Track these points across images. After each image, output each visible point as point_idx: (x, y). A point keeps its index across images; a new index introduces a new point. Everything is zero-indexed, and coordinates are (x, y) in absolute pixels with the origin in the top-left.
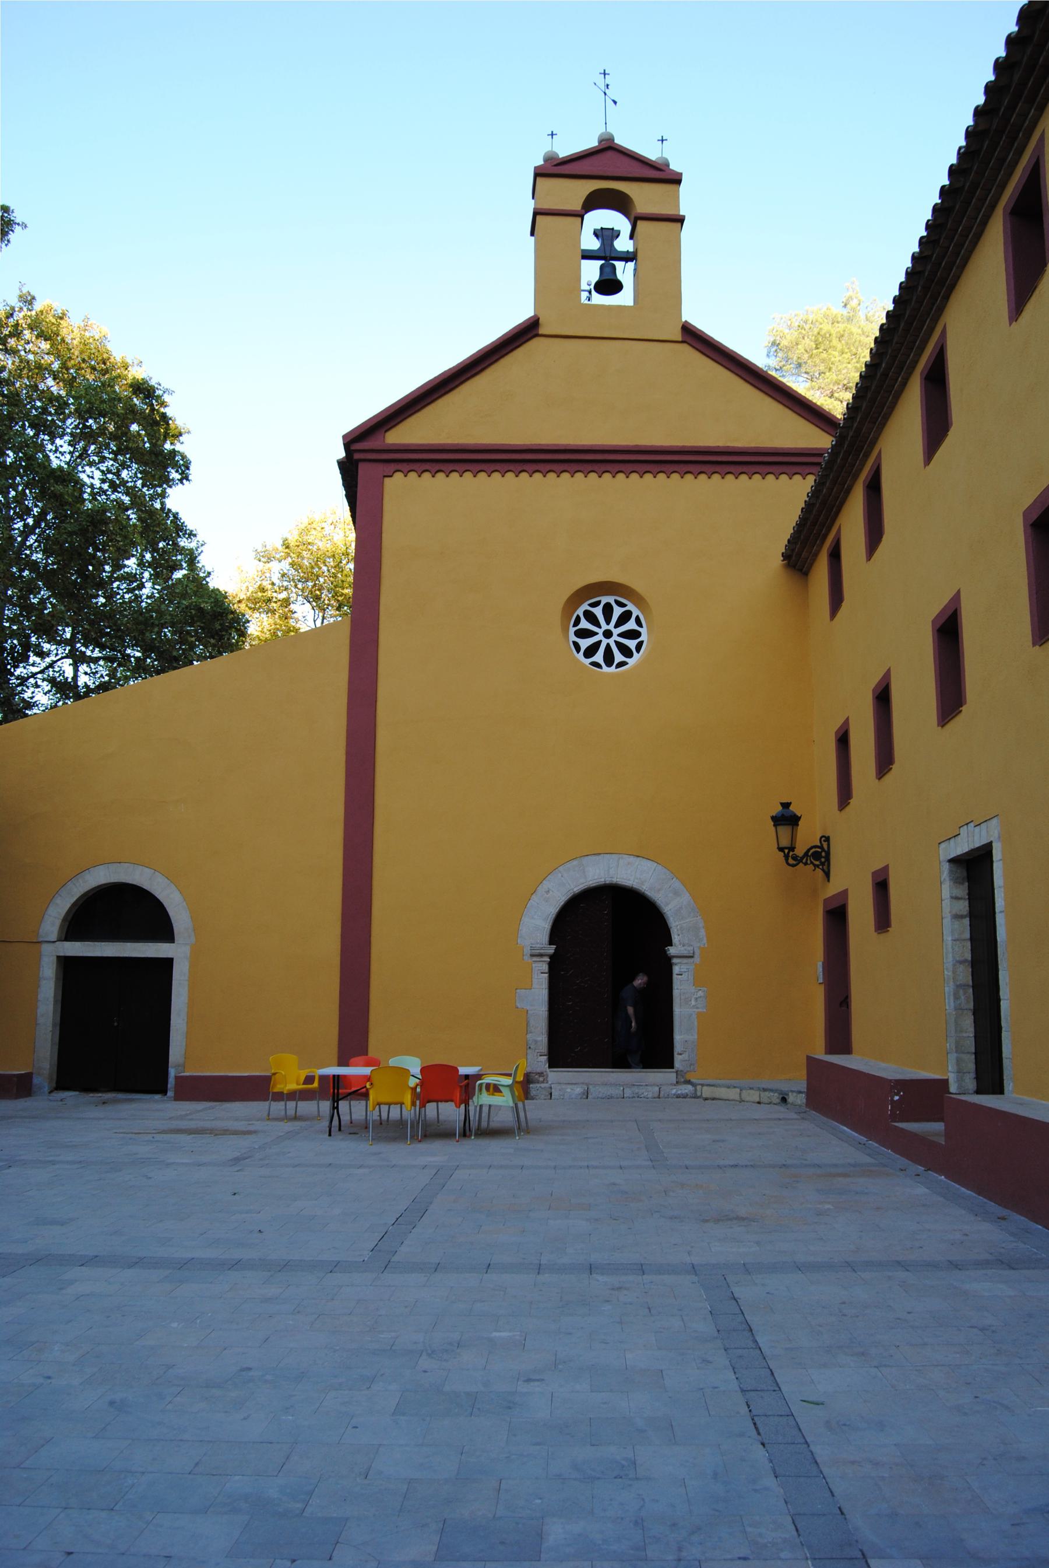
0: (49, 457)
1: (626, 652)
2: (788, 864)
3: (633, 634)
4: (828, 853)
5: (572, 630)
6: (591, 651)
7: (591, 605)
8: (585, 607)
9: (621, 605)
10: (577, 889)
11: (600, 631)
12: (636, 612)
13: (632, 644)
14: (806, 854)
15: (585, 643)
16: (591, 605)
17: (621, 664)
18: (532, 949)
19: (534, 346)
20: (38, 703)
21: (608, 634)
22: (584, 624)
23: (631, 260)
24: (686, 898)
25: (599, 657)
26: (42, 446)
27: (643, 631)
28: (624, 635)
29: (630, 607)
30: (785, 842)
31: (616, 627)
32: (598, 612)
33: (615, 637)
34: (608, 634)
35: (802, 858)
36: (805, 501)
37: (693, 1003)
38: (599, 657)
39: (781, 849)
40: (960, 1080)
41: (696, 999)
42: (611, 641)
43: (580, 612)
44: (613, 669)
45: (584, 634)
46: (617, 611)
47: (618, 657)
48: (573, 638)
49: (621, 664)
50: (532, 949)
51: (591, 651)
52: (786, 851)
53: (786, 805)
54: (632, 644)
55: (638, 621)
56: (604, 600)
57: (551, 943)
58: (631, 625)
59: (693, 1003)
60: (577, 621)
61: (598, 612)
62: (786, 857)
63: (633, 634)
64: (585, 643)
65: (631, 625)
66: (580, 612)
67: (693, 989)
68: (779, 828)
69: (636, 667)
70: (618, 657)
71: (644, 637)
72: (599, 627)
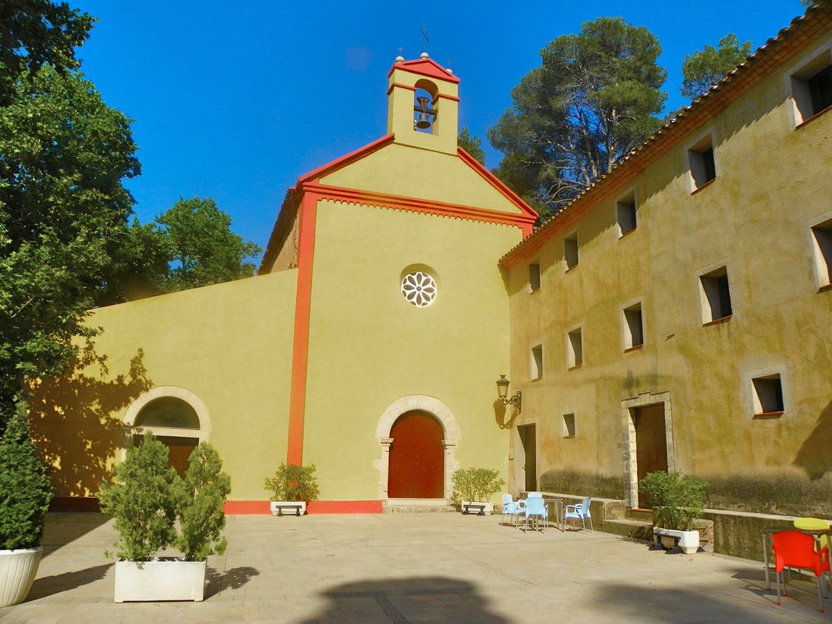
0: (102, 192)
1: (427, 299)
3: (430, 290)
5: (403, 285)
6: (410, 297)
7: (433, 282)
10: (403, 411)
12: (432, 280)
13: (430, 295)
14: (511, 400)
16: (433, 282)
17: (424, 304)
18: (382, 439)
19: (391, 147)
21: (419, 289)
23: (432, 114)
24: (452, 418)
25: (414, 300)
26: (71, 174)
27: (435, 289)
28: (413, 282)
30: (503, 393)
33: (422, 291)
34: (419, 289)
38: (414, 300)
43: (407, 277)
44: (420, 306)
45: (408, 288)
47: (424, 300)
48: (403, 289)
49: (424, 304)
50: (382, 439)
51: (410, 297)
53: (503, 377)
54: (430, 295)
55: (433, 284)
58: (429, 286)
60: (405, 282)
64: (408, 292)
65: (429, 286)
67: (455, 461)
68: (501, 387)
70: (424, 300)
71: (435, 292)
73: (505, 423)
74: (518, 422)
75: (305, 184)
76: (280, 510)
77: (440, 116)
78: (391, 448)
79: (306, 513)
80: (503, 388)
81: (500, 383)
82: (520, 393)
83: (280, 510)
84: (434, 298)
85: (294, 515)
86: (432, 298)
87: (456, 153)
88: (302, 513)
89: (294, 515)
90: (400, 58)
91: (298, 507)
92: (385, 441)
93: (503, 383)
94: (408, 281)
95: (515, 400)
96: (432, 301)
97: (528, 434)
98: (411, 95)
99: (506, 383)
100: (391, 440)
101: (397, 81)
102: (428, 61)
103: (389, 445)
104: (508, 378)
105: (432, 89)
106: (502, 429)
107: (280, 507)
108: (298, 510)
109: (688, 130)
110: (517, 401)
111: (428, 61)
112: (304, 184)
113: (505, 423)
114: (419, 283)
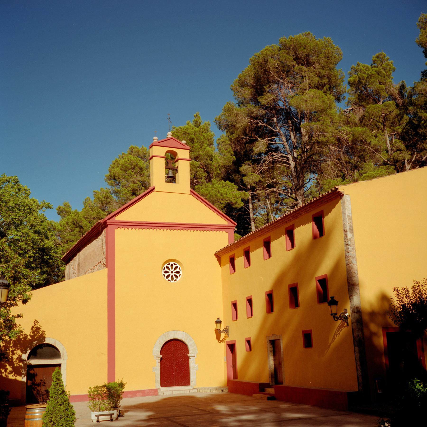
2: (334, 320)
3: (178, 272)
4: (228, 330)
5: (163, 271)
6: (168, 277)
7: (179, 268)
8: (166, 265)
9: (175, 264)
11: (170, 271)
12: (179, 266)
14: (223, 330)
15: (166, 275)
17: (175, 280)
20: (240, 261)
21: (172, 272)
22: (166, 270)
27: (181, 271)
28: (176, 272)
29: (177, 265)
31: (174, 270)
32: (169, 266)
33: (174, 273)
34: (172, 272)
35: (339, 318)
36: (303, 226)
37: (195, 368)
39: (332, 314)
40: (272, 383)
41: (196, 367)
42: (173, 274)
46: (174, 266)
48: (163, 273)
49: (175, 280)
52: (334, 315)
53: (218, 319)
54: (178, 275)
56: (171, 263)
57: (161, 354)
59: (195, 368)
61: (169, 266)
62: (334, 317)
63: (178, 272)
64: (166, 275)
66: (165, 266)
69: (172, 283)
71: (181, 273)
72: (170, 270)
73: (221, 339)
74: (227, 339)
75: (108, 221)
76: (98, 418)
77: (180, 170)
78: (161, 360)
79: (117, 419)
80: (219, 325)
81: (217, 322)
82: (228, 326)
83: (98, 418)
84: (181, 276)
85: (109, 420)
86: (180, 270)
87: (189, 192)
88: (114, 419)
89: (109, 420)
90: (155, 138)
91: (111, 415)
92: (158, 357)
93: (218, 322)
94: (166, 269)
95: (225, 331)
96: (179, 278)
97: (232, 347)
98: (163, 161)
99: (220, 322)
100: (161, 356)
101: (155, 154)
102: (172, 139)
103: (160, 359)
104: (221, 319)
105: (175, 154)
106: (220, 343)
107: (97, 416)
108: (111, 417)
109: (286, 222)
110: (226, 331)
111: (172, 139)
112: (107, 221)
113: (221, 339)
114: (172, 269)
